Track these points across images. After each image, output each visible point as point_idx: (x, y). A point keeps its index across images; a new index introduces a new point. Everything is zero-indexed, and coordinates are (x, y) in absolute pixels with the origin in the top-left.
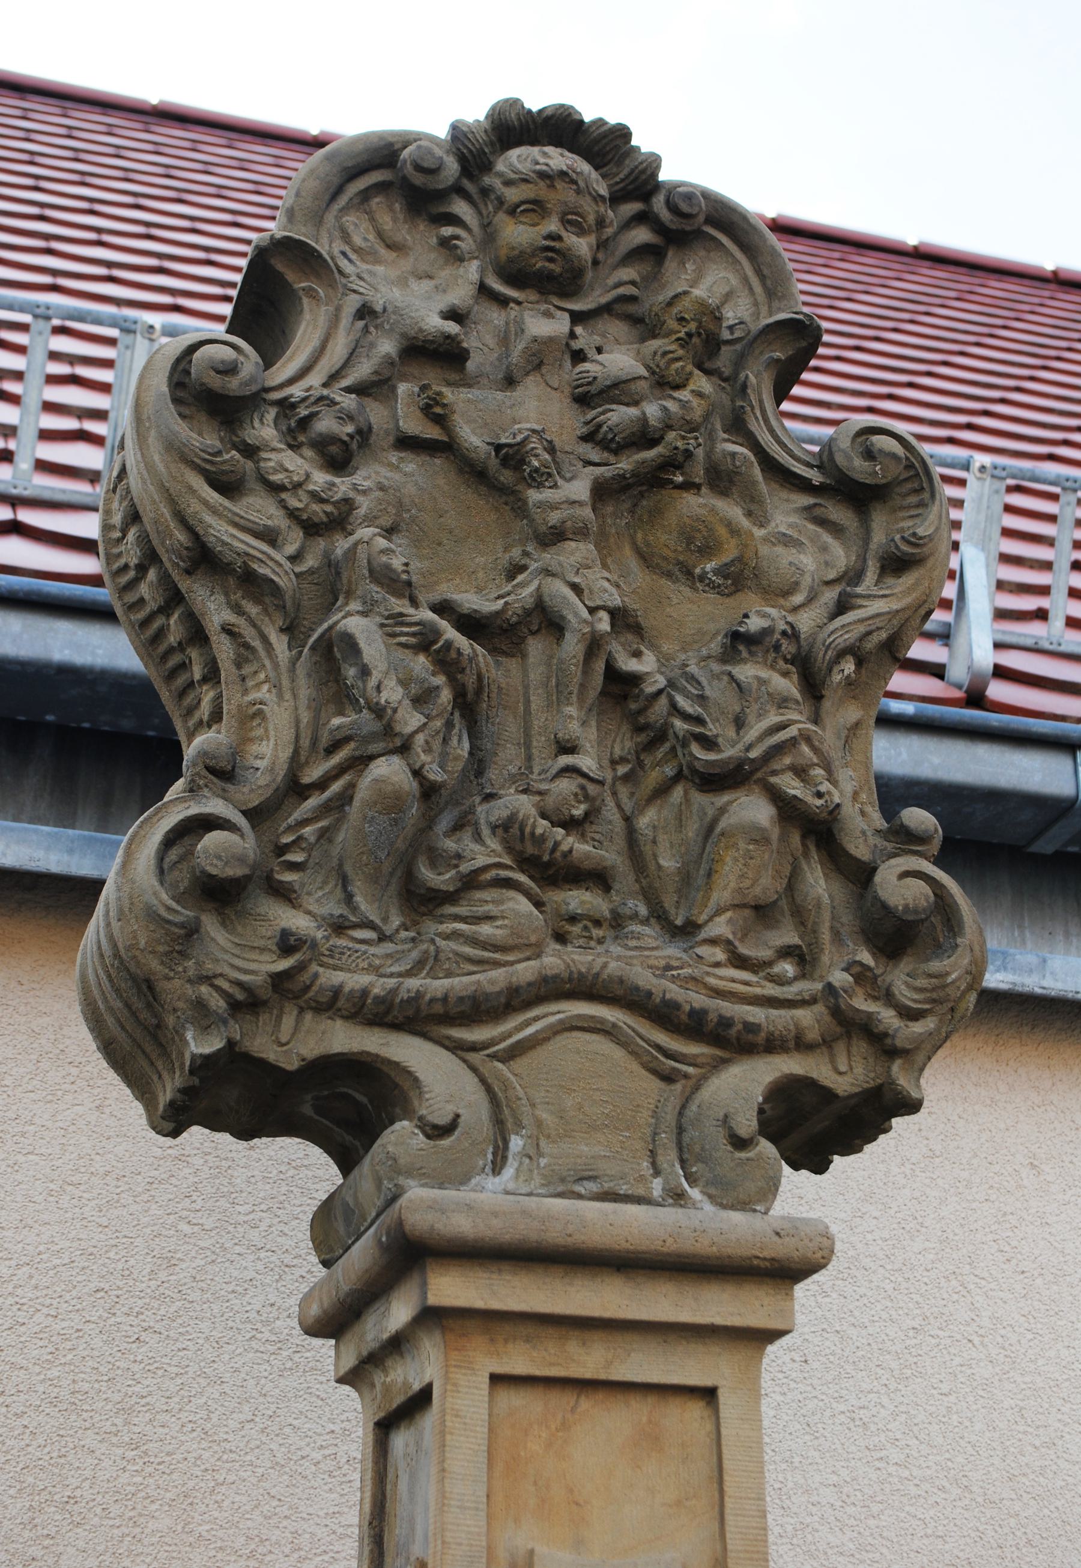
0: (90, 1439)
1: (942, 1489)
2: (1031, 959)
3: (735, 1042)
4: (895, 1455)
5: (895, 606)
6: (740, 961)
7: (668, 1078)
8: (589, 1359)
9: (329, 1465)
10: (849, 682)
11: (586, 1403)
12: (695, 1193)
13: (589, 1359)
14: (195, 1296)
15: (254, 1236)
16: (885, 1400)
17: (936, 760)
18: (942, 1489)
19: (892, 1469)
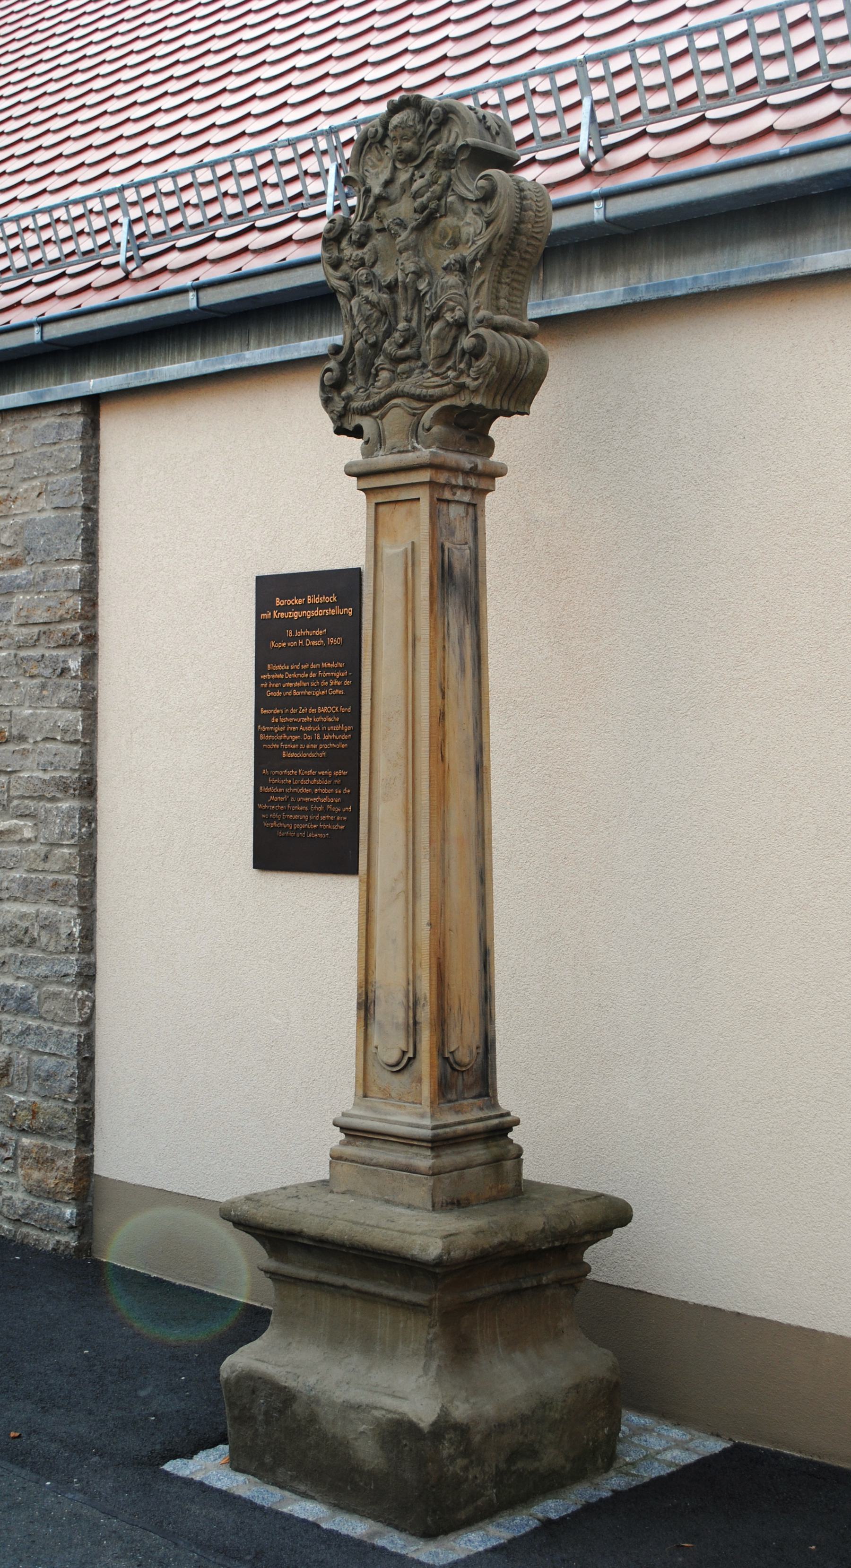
0: (540, 502)
1: (789, 478)
2: (798, 260)
3: (431, 400)
4: (773, 467)
5: (484, 240)
6: (437, 375)
7: (414, 415)
8: (394, 496)
9: (601, 500)
10: (480, 269)
11: (397, 506)
12: (419, 446)
13: (394, 496)
14: (564, 451)
15: (579, 427)
16: (771, 448)
17: (805, 168)
18: (789, 478)
19: (772, 473)
